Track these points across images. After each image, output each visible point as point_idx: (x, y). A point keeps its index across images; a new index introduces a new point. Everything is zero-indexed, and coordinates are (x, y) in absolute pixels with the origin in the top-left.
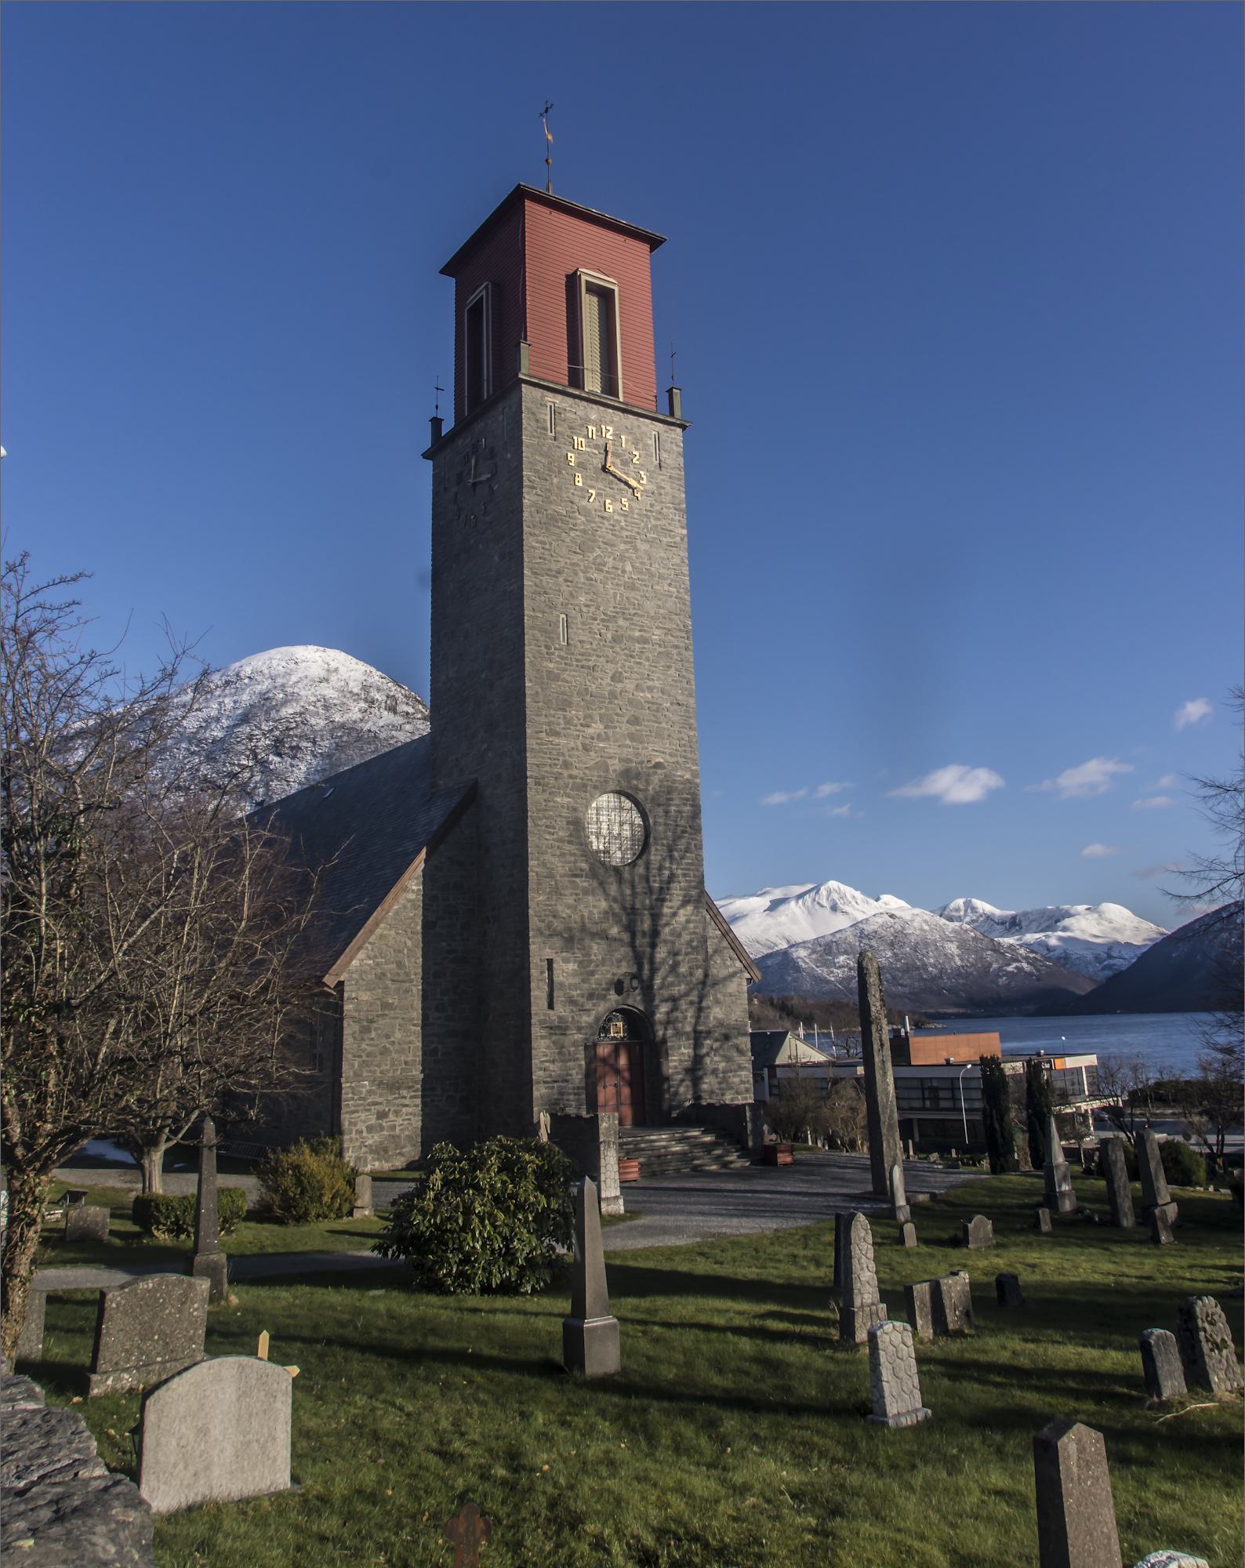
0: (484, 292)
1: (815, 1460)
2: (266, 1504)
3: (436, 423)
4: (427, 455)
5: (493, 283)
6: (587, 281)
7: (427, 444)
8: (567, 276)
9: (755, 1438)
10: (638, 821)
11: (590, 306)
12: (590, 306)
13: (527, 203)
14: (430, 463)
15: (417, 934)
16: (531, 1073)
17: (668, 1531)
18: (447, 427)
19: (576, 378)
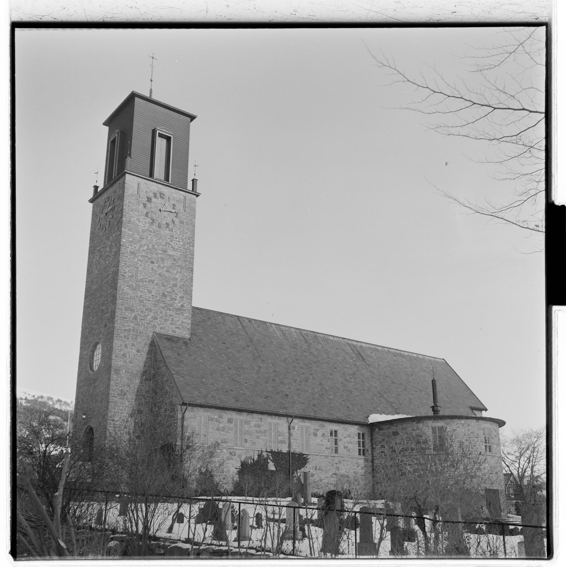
0: (117, 135)
1: (358, 515)
2: (148, 356)
3: (96, 188)
4: (91, 201)
5: (121, 131)
6: (159, 133)
7: (91, 195)
8: (152, 130)
9: (349, 482)
10: (50, 444)
11: (161, 144)
12: (161, 144)
13: (136, 98)
14: (91, 204)
15: (20, 422)
16: (16, 483)
17: (70, 552)
18: (101, 187)
19: (151, 174)
